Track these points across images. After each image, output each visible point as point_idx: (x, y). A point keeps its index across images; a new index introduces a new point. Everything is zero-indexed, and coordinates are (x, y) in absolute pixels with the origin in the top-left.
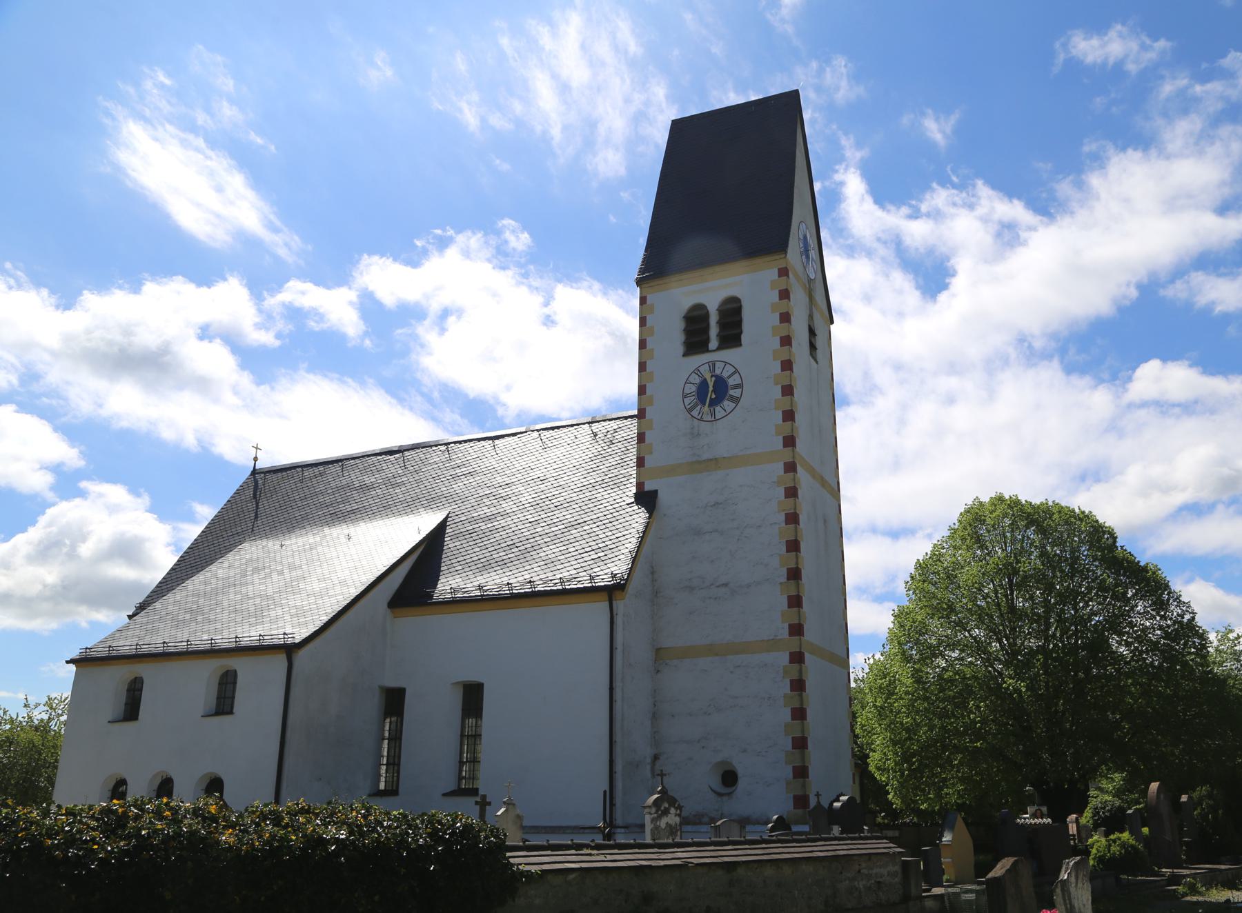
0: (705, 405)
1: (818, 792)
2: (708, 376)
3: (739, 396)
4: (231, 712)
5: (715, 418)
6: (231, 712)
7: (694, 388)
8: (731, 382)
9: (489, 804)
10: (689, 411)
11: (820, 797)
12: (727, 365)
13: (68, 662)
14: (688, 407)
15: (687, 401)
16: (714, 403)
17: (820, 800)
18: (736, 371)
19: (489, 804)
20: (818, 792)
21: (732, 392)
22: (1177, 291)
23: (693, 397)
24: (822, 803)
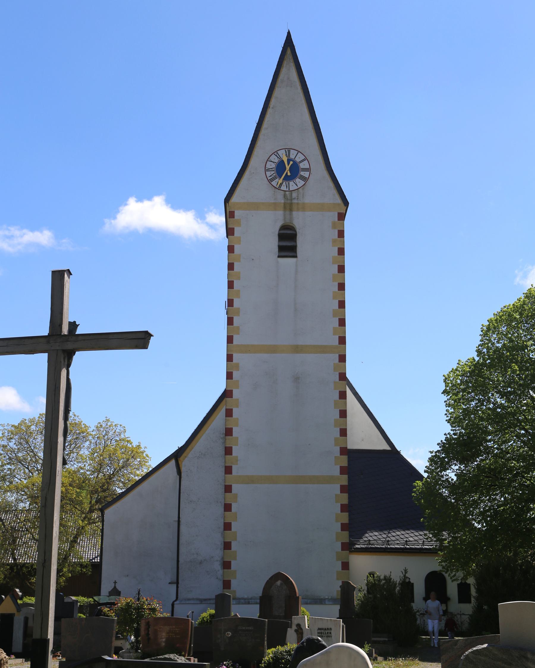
0: (281, 178)
1: (115, 581)
2: (285, 160)
3: (307, 177)
4: (54, 272)
5: (289, 189)
6: (54, 272)
7: (274, 166)
8: (302, 166)
9: (117, 582)
10: (270, 181)
11: (116, 584)
12: (299, 153)
13: (79, 324)
14: (269, 178)
15: (269, 174)
16: (287, 178)
17: (116, 586)
18: (306, 159)
19: (117, 582)
20: (115, 581)
21: (302, 173)
22: (472, 596)
23: (273, 172)
24: (117, 587)
